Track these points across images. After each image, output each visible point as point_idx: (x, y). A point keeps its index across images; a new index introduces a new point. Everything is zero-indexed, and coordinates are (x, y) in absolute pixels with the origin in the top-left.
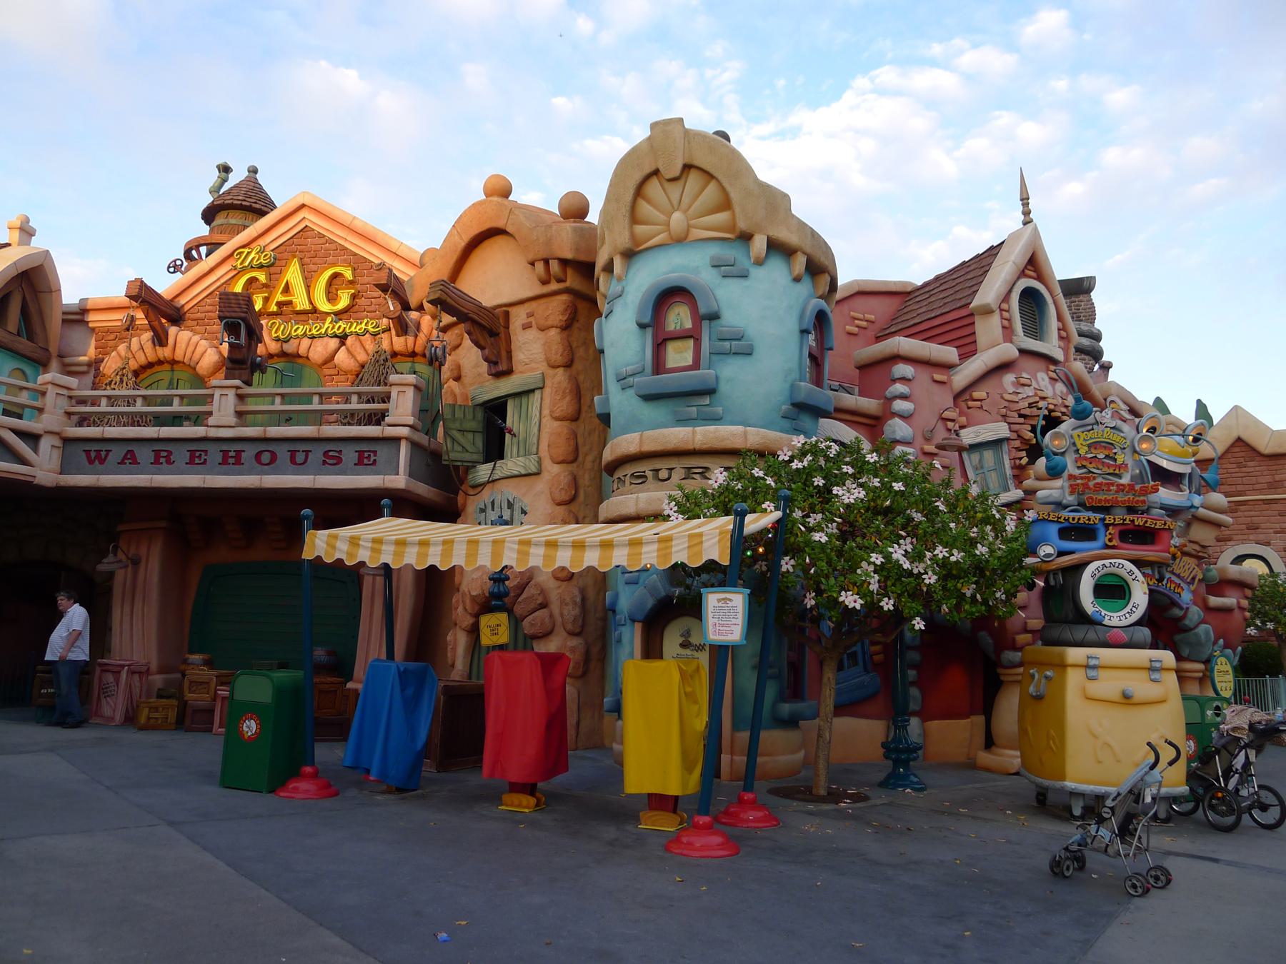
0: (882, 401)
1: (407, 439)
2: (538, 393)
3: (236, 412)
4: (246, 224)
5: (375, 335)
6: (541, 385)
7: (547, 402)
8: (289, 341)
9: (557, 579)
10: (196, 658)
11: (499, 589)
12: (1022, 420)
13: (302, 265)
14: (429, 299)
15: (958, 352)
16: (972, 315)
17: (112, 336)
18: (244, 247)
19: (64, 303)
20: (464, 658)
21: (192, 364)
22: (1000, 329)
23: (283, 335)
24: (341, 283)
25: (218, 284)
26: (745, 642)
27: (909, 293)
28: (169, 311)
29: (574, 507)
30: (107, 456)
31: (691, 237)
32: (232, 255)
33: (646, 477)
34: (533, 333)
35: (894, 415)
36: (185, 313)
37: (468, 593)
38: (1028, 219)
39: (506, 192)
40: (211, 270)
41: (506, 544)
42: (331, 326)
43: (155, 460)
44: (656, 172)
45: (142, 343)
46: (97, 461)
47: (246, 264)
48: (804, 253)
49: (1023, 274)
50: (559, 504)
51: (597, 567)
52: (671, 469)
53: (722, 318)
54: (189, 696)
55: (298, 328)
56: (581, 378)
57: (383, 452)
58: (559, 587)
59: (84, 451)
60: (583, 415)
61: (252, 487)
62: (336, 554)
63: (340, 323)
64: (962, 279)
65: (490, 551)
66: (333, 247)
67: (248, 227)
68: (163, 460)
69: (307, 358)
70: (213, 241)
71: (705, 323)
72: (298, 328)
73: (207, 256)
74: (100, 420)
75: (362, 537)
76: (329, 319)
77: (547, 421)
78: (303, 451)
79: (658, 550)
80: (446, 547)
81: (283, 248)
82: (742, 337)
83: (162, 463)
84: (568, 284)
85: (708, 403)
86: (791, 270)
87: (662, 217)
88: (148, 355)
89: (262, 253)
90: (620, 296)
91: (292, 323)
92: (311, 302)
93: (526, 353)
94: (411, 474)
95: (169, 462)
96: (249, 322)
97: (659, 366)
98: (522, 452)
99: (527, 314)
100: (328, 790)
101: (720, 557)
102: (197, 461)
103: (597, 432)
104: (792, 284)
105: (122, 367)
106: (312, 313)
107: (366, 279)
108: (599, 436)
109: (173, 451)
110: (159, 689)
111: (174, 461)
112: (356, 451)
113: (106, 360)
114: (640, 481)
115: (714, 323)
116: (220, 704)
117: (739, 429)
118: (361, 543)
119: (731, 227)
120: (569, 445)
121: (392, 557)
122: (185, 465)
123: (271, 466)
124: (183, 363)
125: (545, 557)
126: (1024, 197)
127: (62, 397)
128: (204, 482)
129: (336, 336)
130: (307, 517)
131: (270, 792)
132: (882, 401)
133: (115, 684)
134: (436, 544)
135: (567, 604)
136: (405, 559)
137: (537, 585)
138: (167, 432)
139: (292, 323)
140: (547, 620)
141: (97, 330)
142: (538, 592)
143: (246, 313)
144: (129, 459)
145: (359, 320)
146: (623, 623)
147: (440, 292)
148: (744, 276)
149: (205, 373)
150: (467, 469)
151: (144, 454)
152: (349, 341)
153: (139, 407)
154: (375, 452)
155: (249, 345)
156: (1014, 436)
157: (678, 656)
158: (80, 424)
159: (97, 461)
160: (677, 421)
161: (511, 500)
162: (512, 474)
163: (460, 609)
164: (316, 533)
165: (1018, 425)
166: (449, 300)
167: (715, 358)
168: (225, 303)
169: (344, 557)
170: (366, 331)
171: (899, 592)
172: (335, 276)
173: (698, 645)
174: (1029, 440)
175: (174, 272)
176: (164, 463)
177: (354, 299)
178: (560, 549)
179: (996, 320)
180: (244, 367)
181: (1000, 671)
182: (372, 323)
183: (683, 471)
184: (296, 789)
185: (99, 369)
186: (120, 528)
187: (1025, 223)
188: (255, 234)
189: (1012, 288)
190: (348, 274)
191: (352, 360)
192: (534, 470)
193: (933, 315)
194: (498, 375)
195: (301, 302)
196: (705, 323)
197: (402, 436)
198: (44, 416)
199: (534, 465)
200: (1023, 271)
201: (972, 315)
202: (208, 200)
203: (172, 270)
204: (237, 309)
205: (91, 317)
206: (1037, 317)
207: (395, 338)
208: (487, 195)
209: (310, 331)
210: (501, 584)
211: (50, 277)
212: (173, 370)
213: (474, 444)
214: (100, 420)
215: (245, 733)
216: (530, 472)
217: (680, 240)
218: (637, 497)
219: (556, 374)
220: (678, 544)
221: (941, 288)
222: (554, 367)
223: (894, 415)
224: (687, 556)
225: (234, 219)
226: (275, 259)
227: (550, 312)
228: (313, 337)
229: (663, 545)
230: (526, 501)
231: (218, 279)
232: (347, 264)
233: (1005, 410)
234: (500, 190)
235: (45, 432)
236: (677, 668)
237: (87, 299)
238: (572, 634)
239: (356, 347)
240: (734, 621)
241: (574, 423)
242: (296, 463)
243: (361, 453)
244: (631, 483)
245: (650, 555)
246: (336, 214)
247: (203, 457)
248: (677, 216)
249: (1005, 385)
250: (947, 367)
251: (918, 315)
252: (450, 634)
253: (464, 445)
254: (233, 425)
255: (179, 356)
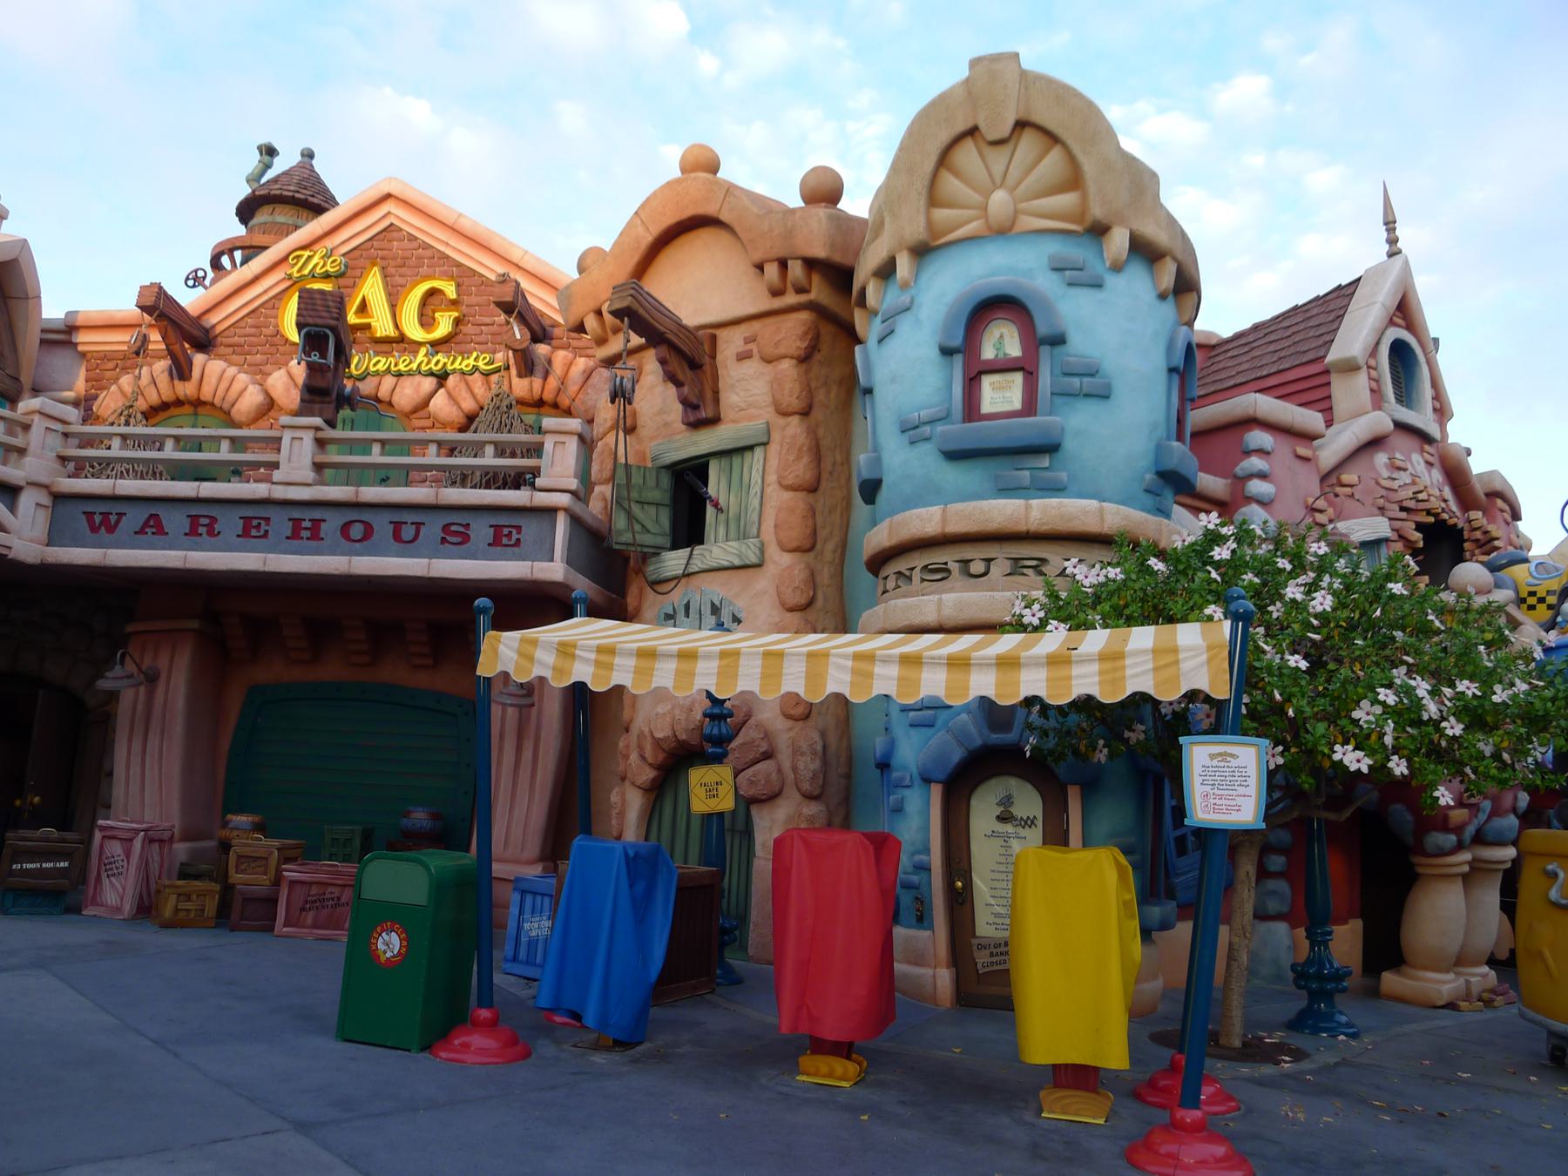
0: (1229, 481)
1: (566, 510)
2: (759, 452)
3: (314, 464)
4: (299, 224)
5: (487, 375)
6: (765, 440)
7: (773, 463)
8: (364, 378)
9: (788, 717)
10: (242, 820)
11: (720, 730)
12: (1403, 515)
13: (385, 276)
14: (613, 308)
15: (1324, 417)
16: (1327, 372)
17: (111, 365)
18: (303, 248)
19: (44, 317)
20: (638, 828)
21: (226, 406)
22: (1368, 392)
23: (356, 369)
24: (439, 302)
25: (265, 298)
26: (1263, 826)
27: (1213, 347)
28: (196, 332)
29: (811, 615)
30: (118, 522)
31: (1019, 227)
32: (285, 259)
33: (948, 571)
34: (752, 367)
35: (1250, 499)
36: (216, 336)
37: (648, 734)
38: (1395, 250)
39: (713, 167)
40: (256, 279)
41: (832, 659)
42: (426, 360)
43: (191, 530)
44: (973, 132)
45: (155, 375)
46: (103, 530)
47: (306, 272)
48: (1175, 259)
49: (1391, 323)
50: (791, 610)
51: (993, 698)
52: (988, 561)
53: (1068, 343)
54: (236, 877)
55: (379, 362)
56: (821, 432)
57: (530, 528)
58: (791, 729)
59: (84, 513)
60: (823, 484)
61: (336, 572)
62: (534, 669)
63: (439, 356)
64: (1301, 327)
65: (804, 669)
66: (428, 253)
67: (300, 227)
68: (202, 530)
69: (390, 404)
70: (254, 244)
71: (1045, 351)
72: (379, 362)
73: (242, 264)
74: (103, 467)
75: (580, 643)
76: (423, 351)
77: (773, 491)
78: (412, 523)
79: (1101, 673)
80: (725, 662)
81: (357, 253)
82: (1097, 372)
83: (201, 535)
84: (812, 296)
85: (1046, 464)
86: (1155, 281)
87: (976, 198)
88: (162, 391)
89: (329, 258)
90: (908, 309)
91: (369, 355)
92: (397, 326)
93: (742, 394)
94: (570, 561)
95: (211, 533)
96: (339, 334)
97: (971, 409)
98: (733, 533)
99: (745, 339)
100: (517, 1049)
101: (1212, 684)
102: (254, 532)
103: (839, 510)
104: (1157, 303)
105: (128, 404)
106: (397, 342)
107: (474, 299)
108: (842, 515)
109: (218, 517)
110: (181, 864)
111: (219, 533)
112: (491, 526)
113: (100, 398)
114: (939, 576)
115: (1058, 350)
116: (286, 891)
117: (1092, 504)
118: (578, 652)
119: (1079, 215)
120: (806, 526)
121: (632, 675)
122: (235, 537)
123: (365, 543)
124: (213, 404)
125: (901, 680)
126: (1391, 219)
127: (54, 434)
128: (265, 564)
129: (431, 374)
130: (484, 611)
131: (423, 1049)
132: (1229, 481)
133: (123, 857)
134: (708, 656)
135: (803, 754)
136: (654, 679)
137: (758, 725)
138: (208, 489)
139: (369, 355)
140: (774, 776)
141: (89, 355)
142: (761, 736)
143: (337, 319)
144: (151, 526)
145: (465, 354)
146: (907, 782)
147: (630, 298)
148: (1097, 285)
149: (244, 419)
150: (645, 558)
151: (175, 521)
152: (451, 381)
153: (169, 452)
154: (519, 528)
155: (336, 368)
156: (1393, 536)
157: (994, 834)
158: (75, 475)
159: (103, 530)
160: (1000, 490)
161: (717, 603)
162: (719, 566)
163: (634, 757)
164: (500, 636)
165: (1400, 522)
166: (641, 311)
167: (1058, 400)
168: (307, 303)
169: (548, 674)
170: (476, 368)
171: (1413, 748)
172: (432, 293)
173: (1025, 818)
174: (1416, 542)
175: (194, 286)
176: (204, 535)
177: (457, 325)
178: (925, 668)
179: (1362, 380)
180: (327, 399)
181: (1416, 859)
182: (484, 358)
183: (1008, 563)
184: (466, 1046)
185: (92, 410)
186: (130, 628)
187: (1391, 255)
188: (319, 232)
189: (1380, 339)
190: (450, 290)
191: (455, 408)
192: (754, 559)
193: (1265, 373)
194: (696, 425)
195: (382, 325)
196: (1045, 351)
197: (560, 505)
198: (28, 460)
199: (755, 553)
200: (1391, 319)
201: (1327, 372)
202: (245, 191)
203: (191, 283)
204: (324, 314)
205: (81, 338)
206: (1403, 385)
207: (516, 381)
208: (683, 170)
209: (396, 365)
210: (723, 722)
211: (27, 279)
212: (196, 414)
213: (657, 522)
214: (103, 467)
215: (380, 953)
216: (748, 562)
217: (1002, 231)
218: (940, 600)
219: (788, 425)
220: (1136, 664)
221: (1267, 339)
222: (785, 414)
223: (1250, 499)
224: (1152, 683)
225: (282, 216)
226: (346, 267)
227: (782, 335)
228: (399, 375)
229: (1108, 665)
230: (741, 605)
231: (265, 292)
232: (451, 278)
233: (1382, 500)
234: (703, 164)
235: (28, 483)
236: (1113, 863)
237: (77, 312)
238: (810, 797)
239: (460, 391)
240: (1241, 790)
241: (811, 495)
242: (402, 540)
243: (498, 529)
244: (923, 580)
245: (1088, 680)
246: (434, 209)
247: (264, 527)
248: (999, 198)
249: (1378, 467)
250: (1309, 437)
251: (1238, 373)
252: (614, 792)
253: (644, 523)
254: (310, 481)
255: (206, 394)
